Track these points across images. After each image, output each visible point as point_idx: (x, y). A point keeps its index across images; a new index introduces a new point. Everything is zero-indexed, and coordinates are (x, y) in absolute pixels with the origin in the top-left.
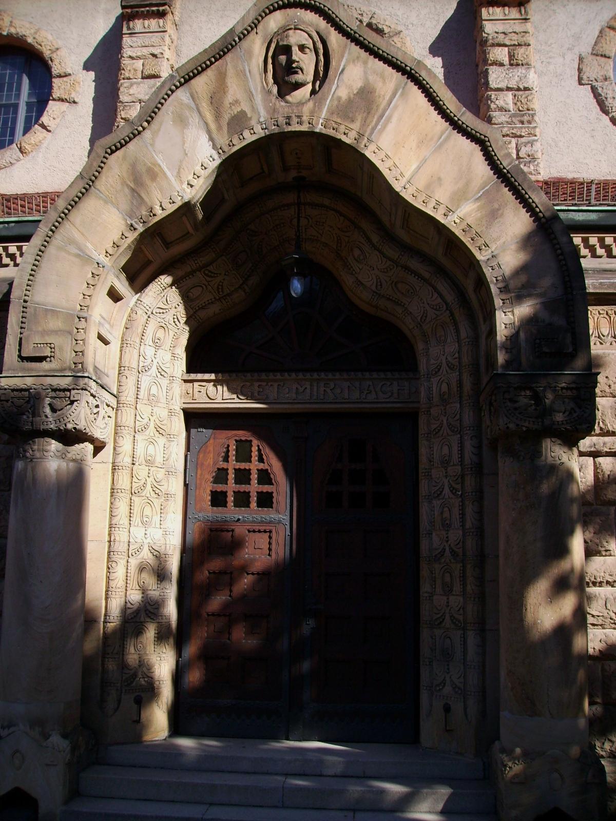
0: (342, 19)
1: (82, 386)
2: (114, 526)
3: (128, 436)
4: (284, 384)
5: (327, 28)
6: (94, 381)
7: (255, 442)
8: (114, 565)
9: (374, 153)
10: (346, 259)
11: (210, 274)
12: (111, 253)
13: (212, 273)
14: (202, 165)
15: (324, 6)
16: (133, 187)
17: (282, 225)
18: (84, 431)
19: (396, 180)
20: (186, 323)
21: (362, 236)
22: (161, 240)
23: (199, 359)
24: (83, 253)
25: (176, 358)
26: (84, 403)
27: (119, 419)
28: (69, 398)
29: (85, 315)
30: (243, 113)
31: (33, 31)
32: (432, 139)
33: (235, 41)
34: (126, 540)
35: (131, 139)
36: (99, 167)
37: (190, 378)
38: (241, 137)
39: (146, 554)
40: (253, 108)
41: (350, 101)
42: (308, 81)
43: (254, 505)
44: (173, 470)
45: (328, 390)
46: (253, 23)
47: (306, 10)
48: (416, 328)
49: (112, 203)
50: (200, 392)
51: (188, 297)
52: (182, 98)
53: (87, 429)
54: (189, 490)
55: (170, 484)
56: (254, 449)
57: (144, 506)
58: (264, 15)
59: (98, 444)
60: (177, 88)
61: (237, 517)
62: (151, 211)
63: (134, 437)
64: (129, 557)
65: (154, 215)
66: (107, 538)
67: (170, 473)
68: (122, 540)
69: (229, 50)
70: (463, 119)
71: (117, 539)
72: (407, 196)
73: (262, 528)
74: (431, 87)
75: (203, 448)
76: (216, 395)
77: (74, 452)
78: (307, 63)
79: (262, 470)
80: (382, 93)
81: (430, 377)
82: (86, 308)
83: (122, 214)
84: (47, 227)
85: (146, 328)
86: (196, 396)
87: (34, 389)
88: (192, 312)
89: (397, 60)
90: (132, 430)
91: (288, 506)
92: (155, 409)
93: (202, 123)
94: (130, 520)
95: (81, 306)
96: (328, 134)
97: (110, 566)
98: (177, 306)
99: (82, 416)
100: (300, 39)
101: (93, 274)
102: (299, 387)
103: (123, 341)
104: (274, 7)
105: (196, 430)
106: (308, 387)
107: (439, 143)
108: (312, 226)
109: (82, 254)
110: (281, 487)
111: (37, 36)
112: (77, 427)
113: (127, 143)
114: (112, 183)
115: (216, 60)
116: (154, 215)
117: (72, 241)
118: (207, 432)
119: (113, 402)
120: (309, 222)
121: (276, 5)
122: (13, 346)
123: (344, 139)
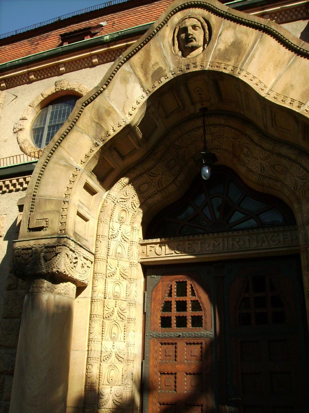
0: (217, 7)
1: (62, 243)
2: (91, 340)
3: (101, 280)
4: (205, 242)
5: (209, 14)
6: (72, 241)
7: (189, 283)
8: (90, 367)
9: (245, 76)
10: (239, 156)
11: (152, 175)
12: (84, 161)
13: (154, 174)
14: (137, 102)
15: (206, 3)
16: (97, 122)
17: (196, 141)
18: (64, 273)
19: (262, 90)
20: (140, 207)
21: (247, 139)
22: (118, 154)
23: (151, 229)
24: (68, 163)
25: (134, 230)
26: (63, 254)
27: (96, 269)
28: (55, 251)
29: (67, 200)
30: (160, 69)
31: (78, 86)
32: (283, 63)
33: (154, 32)
34: (100, 350)
35: (96, 96)
36: (79, 114)
37: (144, 243)
38: (160, 82)
39: (113, 360)
40: (166, 65)
41: (226, 50)
42: (200, 45)
43: (189, 325)
44: (133, 302)
45: (235, 243)
46: (164, 21)
47: (196, 8)
48: (291, 195)
49: (85, 133)
50: (151, 251)
51: (140, 191)
52: (125, 69)
53: (67, 272)
54: (147, 317)
55: (131, 312)
56: (189, 287)
57: (112, 326)
58: (170, 15)
59: (79, 285)
60: (123, 64)
61: (179, 333)
62: (107, 134)
63: (106, 280)
64: (101, 362)
65: (109, 135)
66: (87, 349)
67: (131, 304)
68: (96, 349)
69: (151, 38)
70: (303, 48)
71: (93, 349)
72: (270, 98)
73: (196, 341)
74: (279, 34)
75: (155, 288)
76: (162, 252)
77: (59, 288)
78: (199, 36)
79: (194, 301)
80: (247, 43)
81: (305, 227)
82: (68, 196)
83: (91, 138)
84: (48, 151)
85: (113, 211)
86: (148, 254)
87: (35, 248)
88: (143, 200)
89: (255, 22)
90: (105, 276)
91: (213, 325)
92: (120, 262)
93: (137, 79)
94: (102, 336)
95: (66, 195)
96: (214, 70)
97: (88, 368)
98: (133, 197)
99: (62, 263)
100: (192, 22)
101: (73, 175)
102: (215, 243)
103: (99, 220)
104: (176, 10)
105: (150, 276)
106: (221, 242)
107: (289, 64)
108: (215, 139)
109: (67, 164)
110: (208, 312)
111: (80, 88)
112: (59, 270)
113: (94, 98)
114: (86, 122)
115: (144, 45)
116: (109, 135)
117: (62, 158)
118: (157, 278)
119: (91, 257)
120: (213, 136)
121: (177, 9)
122: (25, 223)
123: (224, 71)
